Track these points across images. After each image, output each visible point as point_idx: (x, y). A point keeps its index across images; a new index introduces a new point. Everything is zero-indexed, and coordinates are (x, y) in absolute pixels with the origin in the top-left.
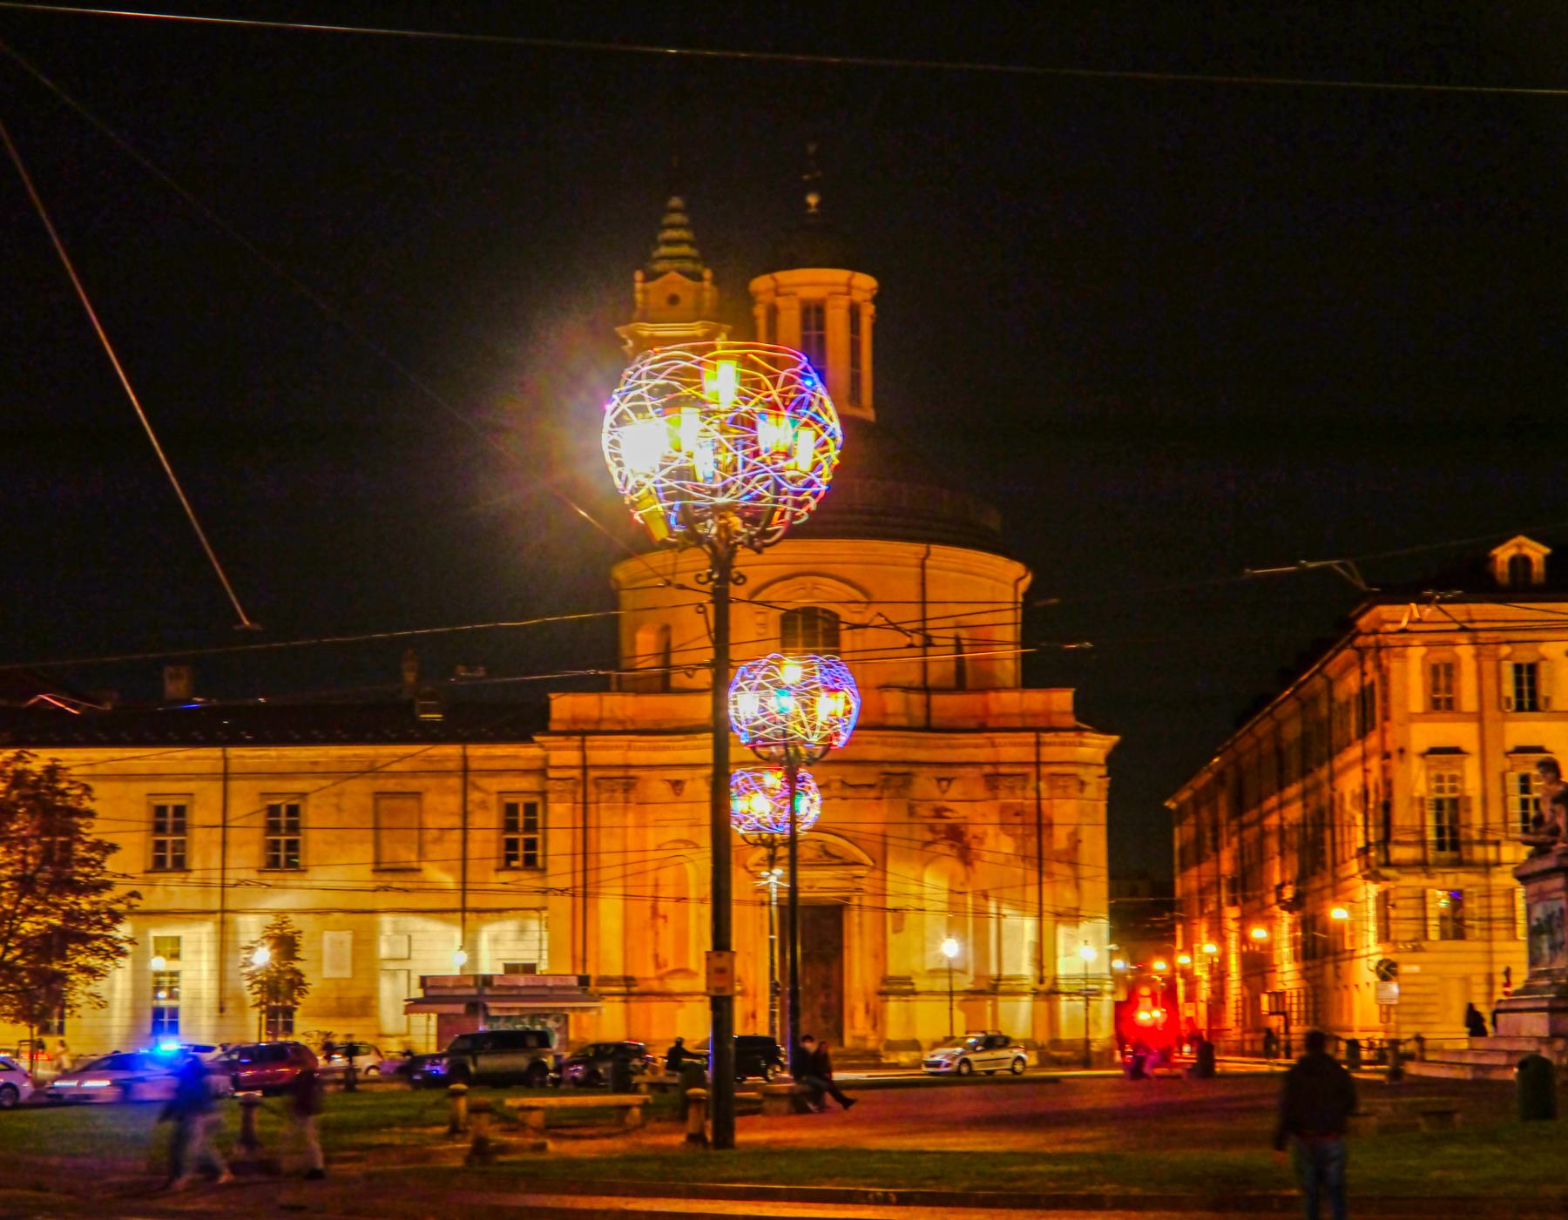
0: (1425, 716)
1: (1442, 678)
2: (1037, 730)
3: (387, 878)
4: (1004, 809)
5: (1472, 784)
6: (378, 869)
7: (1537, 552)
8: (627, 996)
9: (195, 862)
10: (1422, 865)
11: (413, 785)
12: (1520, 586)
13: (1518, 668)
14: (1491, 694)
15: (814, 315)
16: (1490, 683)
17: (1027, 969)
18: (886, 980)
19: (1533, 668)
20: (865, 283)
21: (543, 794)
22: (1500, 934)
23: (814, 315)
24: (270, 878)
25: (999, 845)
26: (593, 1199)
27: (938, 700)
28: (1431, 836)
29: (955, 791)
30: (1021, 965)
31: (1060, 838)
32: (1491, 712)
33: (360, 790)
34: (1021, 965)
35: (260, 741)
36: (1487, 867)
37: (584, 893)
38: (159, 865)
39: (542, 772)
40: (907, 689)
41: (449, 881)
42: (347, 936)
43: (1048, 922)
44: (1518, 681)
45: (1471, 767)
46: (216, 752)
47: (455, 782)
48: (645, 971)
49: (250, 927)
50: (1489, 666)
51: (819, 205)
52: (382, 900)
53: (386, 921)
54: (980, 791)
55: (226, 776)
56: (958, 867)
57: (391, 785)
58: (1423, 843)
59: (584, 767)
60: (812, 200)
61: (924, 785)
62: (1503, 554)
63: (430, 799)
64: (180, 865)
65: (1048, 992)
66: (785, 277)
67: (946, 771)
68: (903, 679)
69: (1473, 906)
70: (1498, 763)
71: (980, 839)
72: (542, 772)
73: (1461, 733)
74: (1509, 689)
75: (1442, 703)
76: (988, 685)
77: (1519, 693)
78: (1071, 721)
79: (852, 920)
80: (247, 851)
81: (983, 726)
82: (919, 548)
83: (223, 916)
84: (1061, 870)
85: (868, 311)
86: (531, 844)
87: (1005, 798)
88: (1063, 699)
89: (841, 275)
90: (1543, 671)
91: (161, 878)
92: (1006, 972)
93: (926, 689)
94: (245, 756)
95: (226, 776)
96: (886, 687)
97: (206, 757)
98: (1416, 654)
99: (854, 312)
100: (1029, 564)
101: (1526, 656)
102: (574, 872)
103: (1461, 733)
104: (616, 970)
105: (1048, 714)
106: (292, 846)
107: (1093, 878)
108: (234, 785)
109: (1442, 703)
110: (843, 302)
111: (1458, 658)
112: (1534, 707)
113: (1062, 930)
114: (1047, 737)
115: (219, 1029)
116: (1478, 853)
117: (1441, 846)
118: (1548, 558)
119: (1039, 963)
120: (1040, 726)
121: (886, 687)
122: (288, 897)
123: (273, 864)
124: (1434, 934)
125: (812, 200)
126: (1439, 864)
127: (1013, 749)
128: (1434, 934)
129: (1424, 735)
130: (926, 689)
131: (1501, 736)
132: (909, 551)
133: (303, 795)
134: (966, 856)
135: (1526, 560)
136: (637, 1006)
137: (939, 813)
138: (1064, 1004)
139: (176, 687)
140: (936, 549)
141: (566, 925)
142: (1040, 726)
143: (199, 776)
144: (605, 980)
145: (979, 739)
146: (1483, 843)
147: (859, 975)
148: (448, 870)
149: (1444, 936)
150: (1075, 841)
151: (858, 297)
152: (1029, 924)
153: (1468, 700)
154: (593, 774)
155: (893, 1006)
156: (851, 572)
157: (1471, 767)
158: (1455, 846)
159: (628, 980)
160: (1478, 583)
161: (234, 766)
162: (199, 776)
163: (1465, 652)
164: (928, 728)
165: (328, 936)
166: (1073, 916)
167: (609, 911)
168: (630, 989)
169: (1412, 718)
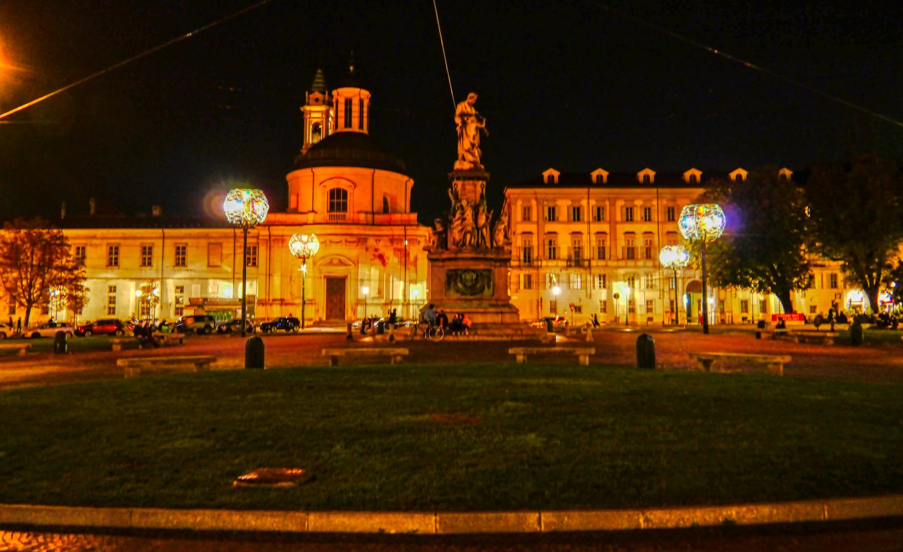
0: (521, 223)
1: (527, 211)
2: (405, 226)
3: (211, 269)
4: (395, 249)
5: (535, 242)
6: (209, 266)
7: (605, 174)
8: (281, 304)
9: (154, 262)
10: (519, 267)
11: (219, 241)
12: (551, 184)
13: (549, 209)
14: (541, 216)
15: (348, 102)
16: (541, 213)
17: (401, 297)
18: (358, 300)
19: (554, 209)
20: (365, 94)
21: (258, 244)
22: (541, 287)
23: (348, 102)
24: (177, 268)
25: (393, 260)
26: (601, 514)
27: (377, 217)
28: (522, 258)
29: (381, 243)
30: (399, 296)
31: (412, 258)
32: (541, 221)
33: (204, 242)
34: (399, 296)
35: (174, 227)
36: (538, 267)
37: (269, 275)
38: (144, 264)
39: (258, 237)
40: (366, 213)
41: (230, 270)
42: (199, 286)
43: (407, 283)
44: (549, 212)
45: (535, 238)
46: (160, 231)
47: (232, 240)
48: (288, 298)
49: (171, 284)
50: (540, 208)
51: (354, 70)
52: (209, 275)
53: (211, 282)
54: (388, 244)
55: (164, 238)
56: (382, 267)
57: (213, 241)
58: (519, 260)
59: (270, 236)
60: (351, 68)
61: (371, 242)
62: (546, 174)
63: (224, 245)
64: (150, 264)
65: (407, 304)
66: (340, 90)
67: (378, 238)
68: (365, 209)
69: (534, 279)
70: (542, 236)
71: (388, 258)
72: (258, 237)
73: (532, 228)
74: (546, 214)
75: (527, 218)
76: (395, 211)
77: (549, 216)
78: (416, 223)
79: (348, 283)
80: (170, 260)
81: (390, 224)
82: (371, 171)
83: (163, 280)
84: (412, 268)
85: (366, 102)
86: (254, 259)
87: (395, 245)
88: (414, 216)
89: (357, 90)
90: (556, 209)
91: (144, 268)
92: (395, 298)
93: (373, 213)
94: (168, 232)
95: (164, 238)
96: (359, 212)
97: (158, 232)
98: (519, 203)
99: (361, 101)
100: (410, 176)
101: (551, 205)
102: (502, 313)
103: (532, 228)
104: (278, 296)
105: (409, 221)
106: (184, 259)
107: (640, 306)
108: (167, 241)
109: (527, 218)
110: (358, 98)
111: (581, 206)
112: (554, 220)
113: (412, 286)
114: (408, 228)
115: (161, 314)
116: (535, 263)
117: (525, 261)
118: (792, 175)
119: (404, 295)
120: (406, 224)
121: (359, 212)
122: (182, 274)
123: (177, 264)
124: (522, 287)
125: (351, 68)
126: (524, 266)
127: (398, 231)
128: (522, 287)
129: (520, 228)
130: (373, 213)
131: (544, 227)
132: (367, 172)
133: (187, 244)
134: (384, 263)
135: (553, 177)
136: (284, 307)
137: (376, 250)
138: (411, 307)
139: (156, 212)
140: (377, 171)
141: (264, 283)
142: (406, 224)
143: (156, 238)
144: (274, 300)
145: (389, 228)
146: (537, 260)
147: (349, 299)
148: (229, 266)
149: (525, 288)
150: (416, 259)
151: (362, 97)
152: (402, 284)
153: (534, 217)
154: (272, 238)
155: (360, 309)
156: (351, 178)
157: (535, 238)
158: (529, 261)
159: (282, 300)
160: (538, 182)
161: (166, 235)
162: (156, 238)
163: (534, 203)
164: (373, 224)
165: (194, 286)
166: (415, 281)
167: (277, 280)
168: (282, 302)
169: (517, 223)
